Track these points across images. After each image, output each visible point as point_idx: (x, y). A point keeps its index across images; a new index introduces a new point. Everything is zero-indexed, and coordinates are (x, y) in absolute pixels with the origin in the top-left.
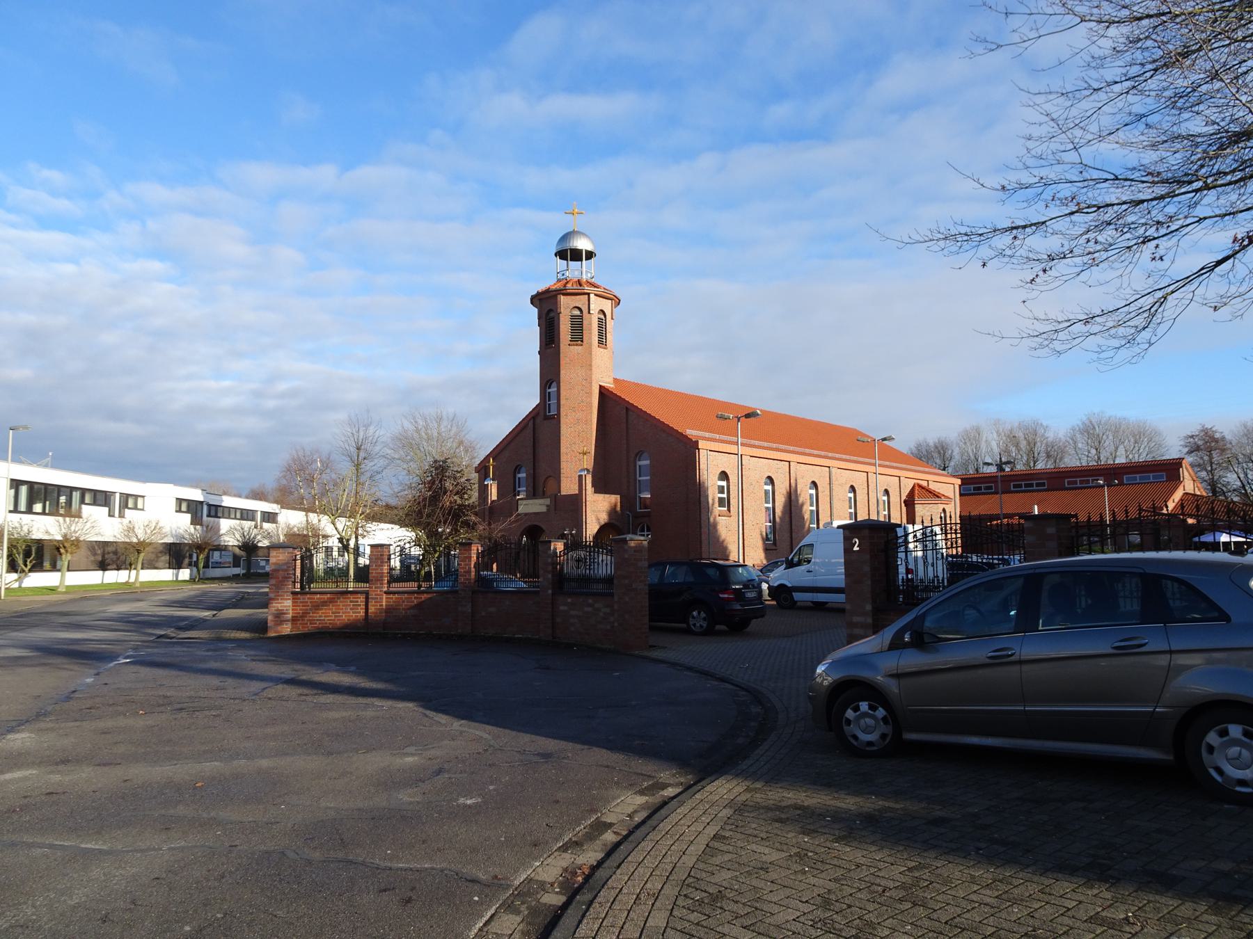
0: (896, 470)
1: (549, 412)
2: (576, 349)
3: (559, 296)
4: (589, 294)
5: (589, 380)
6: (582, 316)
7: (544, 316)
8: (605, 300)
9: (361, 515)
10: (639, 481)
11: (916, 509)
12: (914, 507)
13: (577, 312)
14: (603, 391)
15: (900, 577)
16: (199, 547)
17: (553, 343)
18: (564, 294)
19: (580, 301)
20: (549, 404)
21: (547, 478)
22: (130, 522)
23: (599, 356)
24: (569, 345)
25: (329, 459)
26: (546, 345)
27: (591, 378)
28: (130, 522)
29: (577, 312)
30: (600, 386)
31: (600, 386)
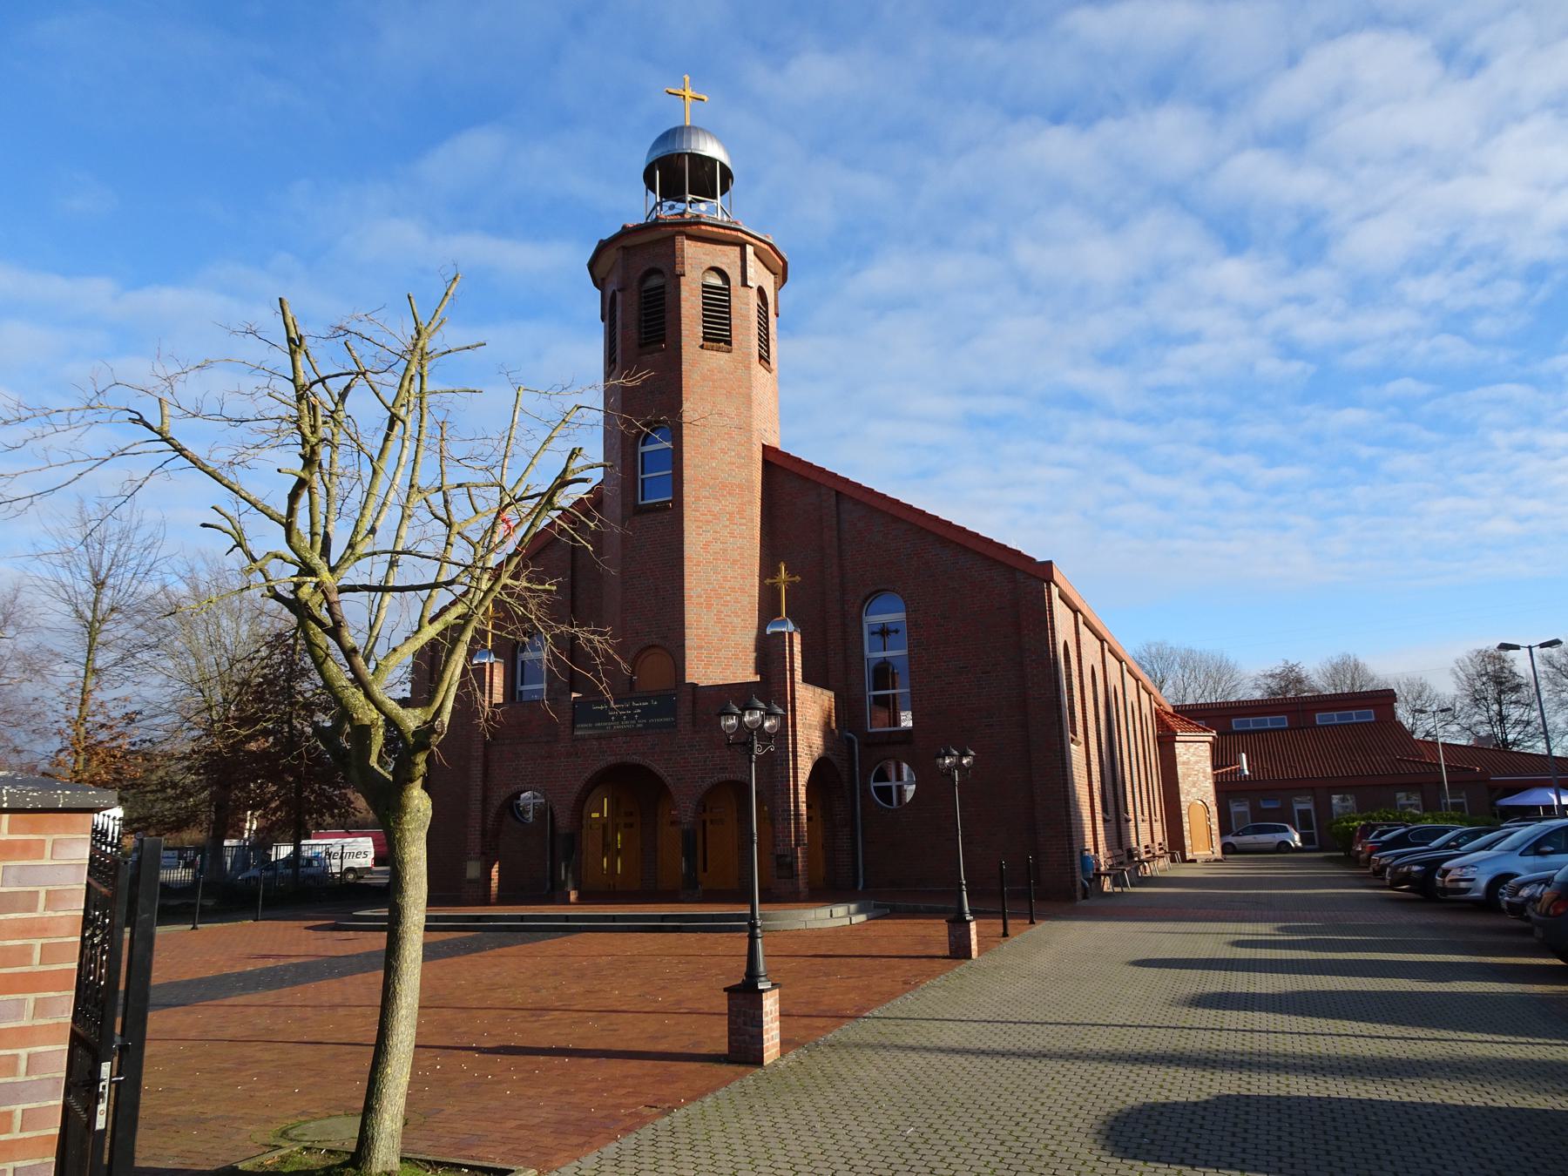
0: (1085, 682)
1: (643, 499)
2: (716, 359)
3: (679, 239)
4: (742, 245)
5: (746, 428)
6: (729, 290)
7: (635, 284)
8: (765, 270)
9: (1174, 660)
10: (521, 692)
11: (1177, 751)
12: (1174, 748)
13: (716, 281)
14: (771, 458)
15: (335, 844)
16: (1131, 854)
17: (663, 341)
18: (690, 237)
19: (727, 258)
20: (643, 480)
21: (642, 651)
22: (580, 449)
23: (763, 382)
24: (702, 347)
25: (12, 602)
26: (641, 346)
27: (750, 425)
28: (580, 449)
29: (716, 281)
30: (764, 445)
31: (764, 445)
